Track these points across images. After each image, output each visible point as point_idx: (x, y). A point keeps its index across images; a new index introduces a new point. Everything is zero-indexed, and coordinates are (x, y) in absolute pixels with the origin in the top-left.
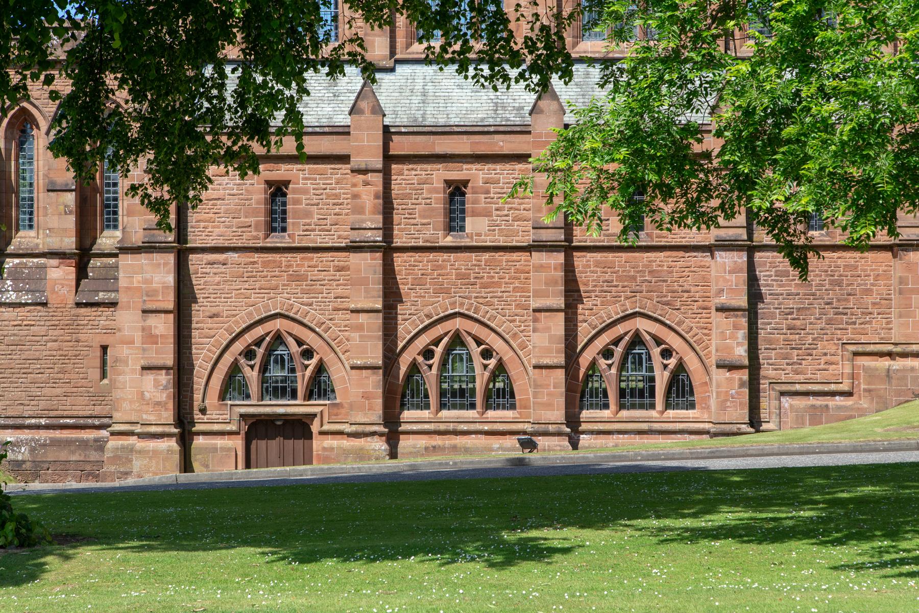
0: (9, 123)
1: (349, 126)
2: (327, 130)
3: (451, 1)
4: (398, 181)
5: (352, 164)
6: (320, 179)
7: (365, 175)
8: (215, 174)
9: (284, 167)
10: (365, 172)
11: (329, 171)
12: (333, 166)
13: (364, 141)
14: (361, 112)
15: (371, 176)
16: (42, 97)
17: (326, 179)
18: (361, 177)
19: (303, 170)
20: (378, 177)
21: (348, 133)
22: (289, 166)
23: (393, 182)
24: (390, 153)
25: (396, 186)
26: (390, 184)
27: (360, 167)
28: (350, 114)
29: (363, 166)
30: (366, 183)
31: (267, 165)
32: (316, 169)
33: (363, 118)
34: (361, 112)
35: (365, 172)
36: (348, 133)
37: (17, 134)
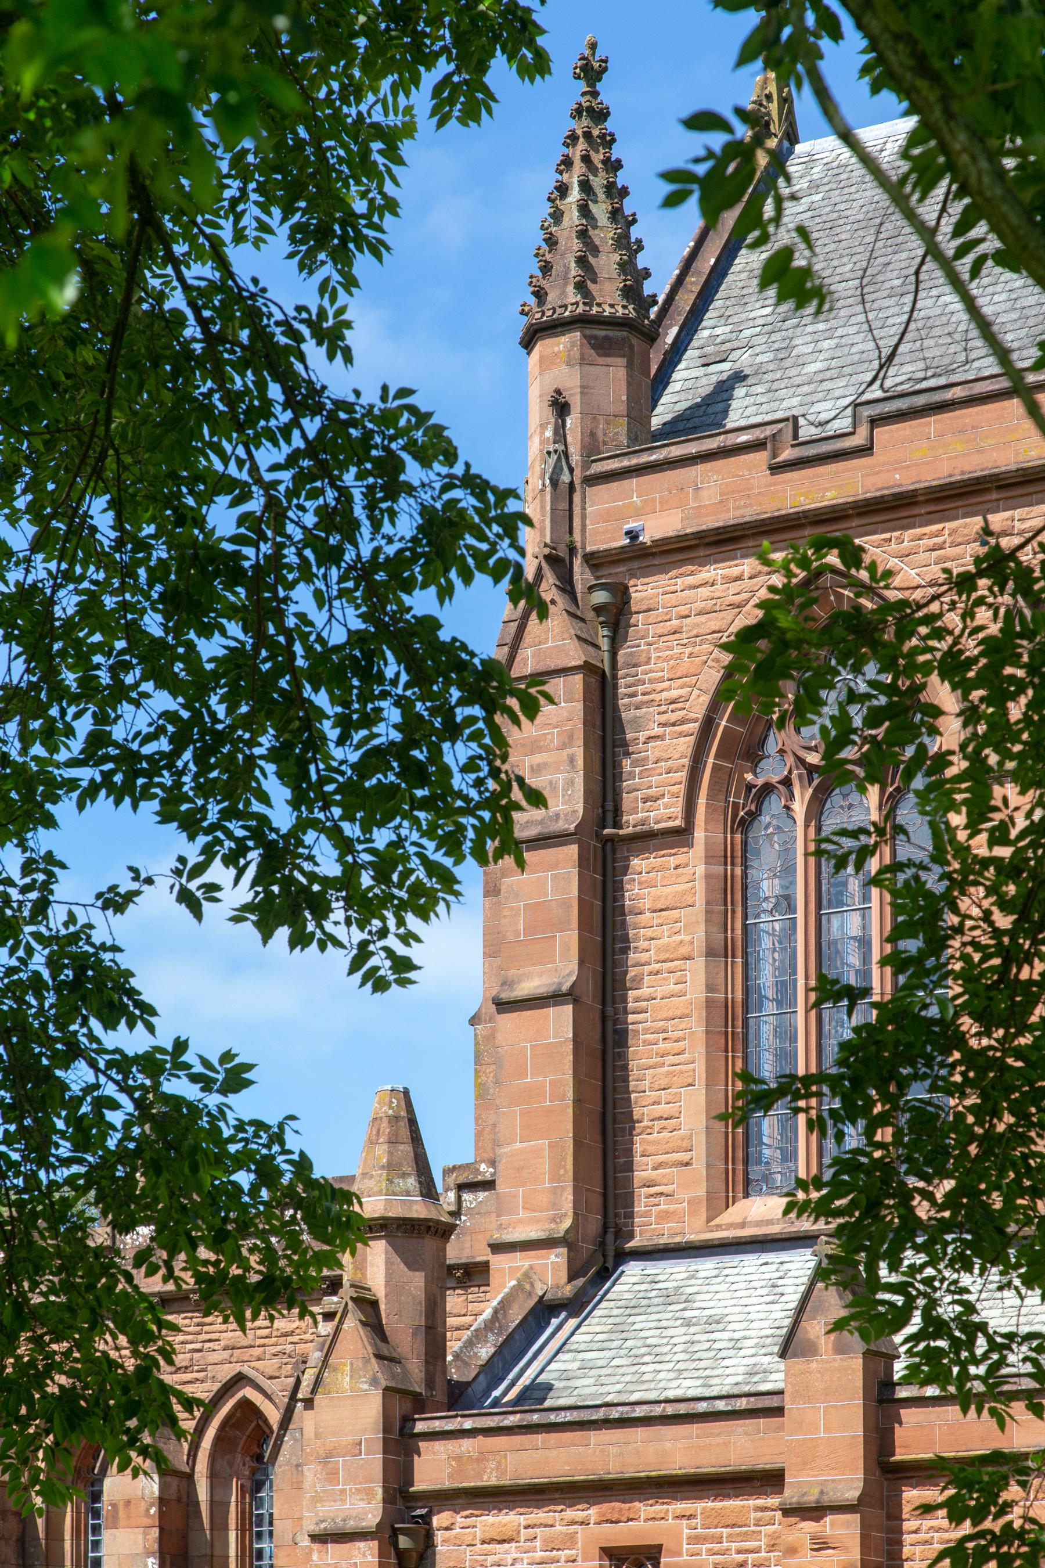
0: (218, 1440)
1: (781, 1393)
2: (742, 1404)
3: (3, 1148)
4: (922, 1536)
5: (788, 1492)
6: (731, 1538)
7: (817, 1519)
8: (488, 1536)
9: (644, 1509)
10: (815, 1512)
11: (753, 1515)
12: (760, 1502)
13: (817, 1430)
14: (810, 1350)
15: (832, 1524)
16: (284, 1372)
17: (746, 1537)
18: (809, 1526)
19: (690, 1517)
20: (848, 1525)
21: (778, 1412)
22: (658, 1507)
23: (907, 1538)
24: (897, 1458)
25: (918, 1549)
26: (900, 1543)
27: (806, 1499)
28: (783, 1354)
29: (811, 1498)
30: (821, 1545)
31: (605, 1506)
32: (720, 1513)
33: (814, 1365)
34: (810, 1350)
35: (815, 1512)
36: (778, 1412)
37: (243, 1464)
